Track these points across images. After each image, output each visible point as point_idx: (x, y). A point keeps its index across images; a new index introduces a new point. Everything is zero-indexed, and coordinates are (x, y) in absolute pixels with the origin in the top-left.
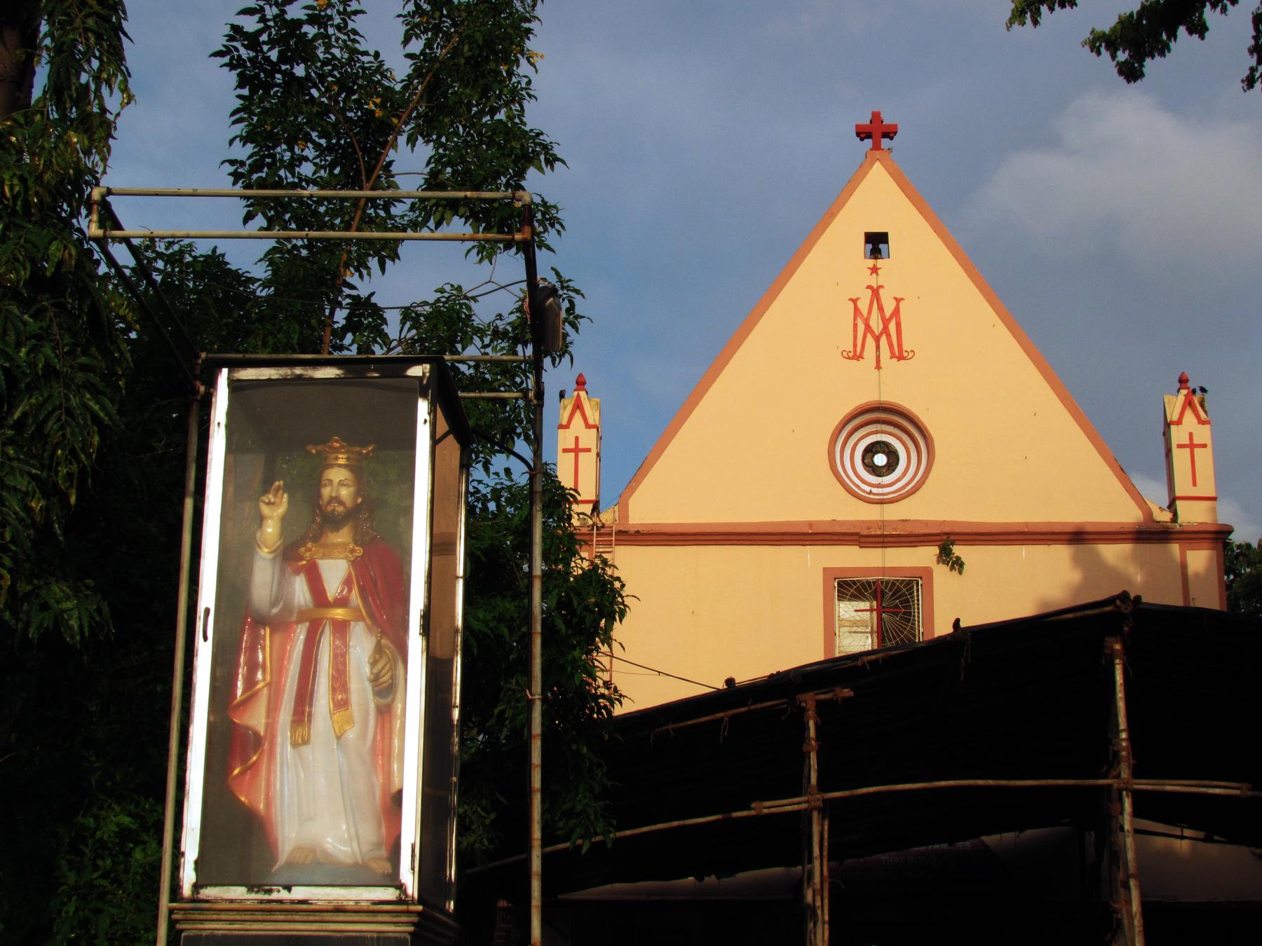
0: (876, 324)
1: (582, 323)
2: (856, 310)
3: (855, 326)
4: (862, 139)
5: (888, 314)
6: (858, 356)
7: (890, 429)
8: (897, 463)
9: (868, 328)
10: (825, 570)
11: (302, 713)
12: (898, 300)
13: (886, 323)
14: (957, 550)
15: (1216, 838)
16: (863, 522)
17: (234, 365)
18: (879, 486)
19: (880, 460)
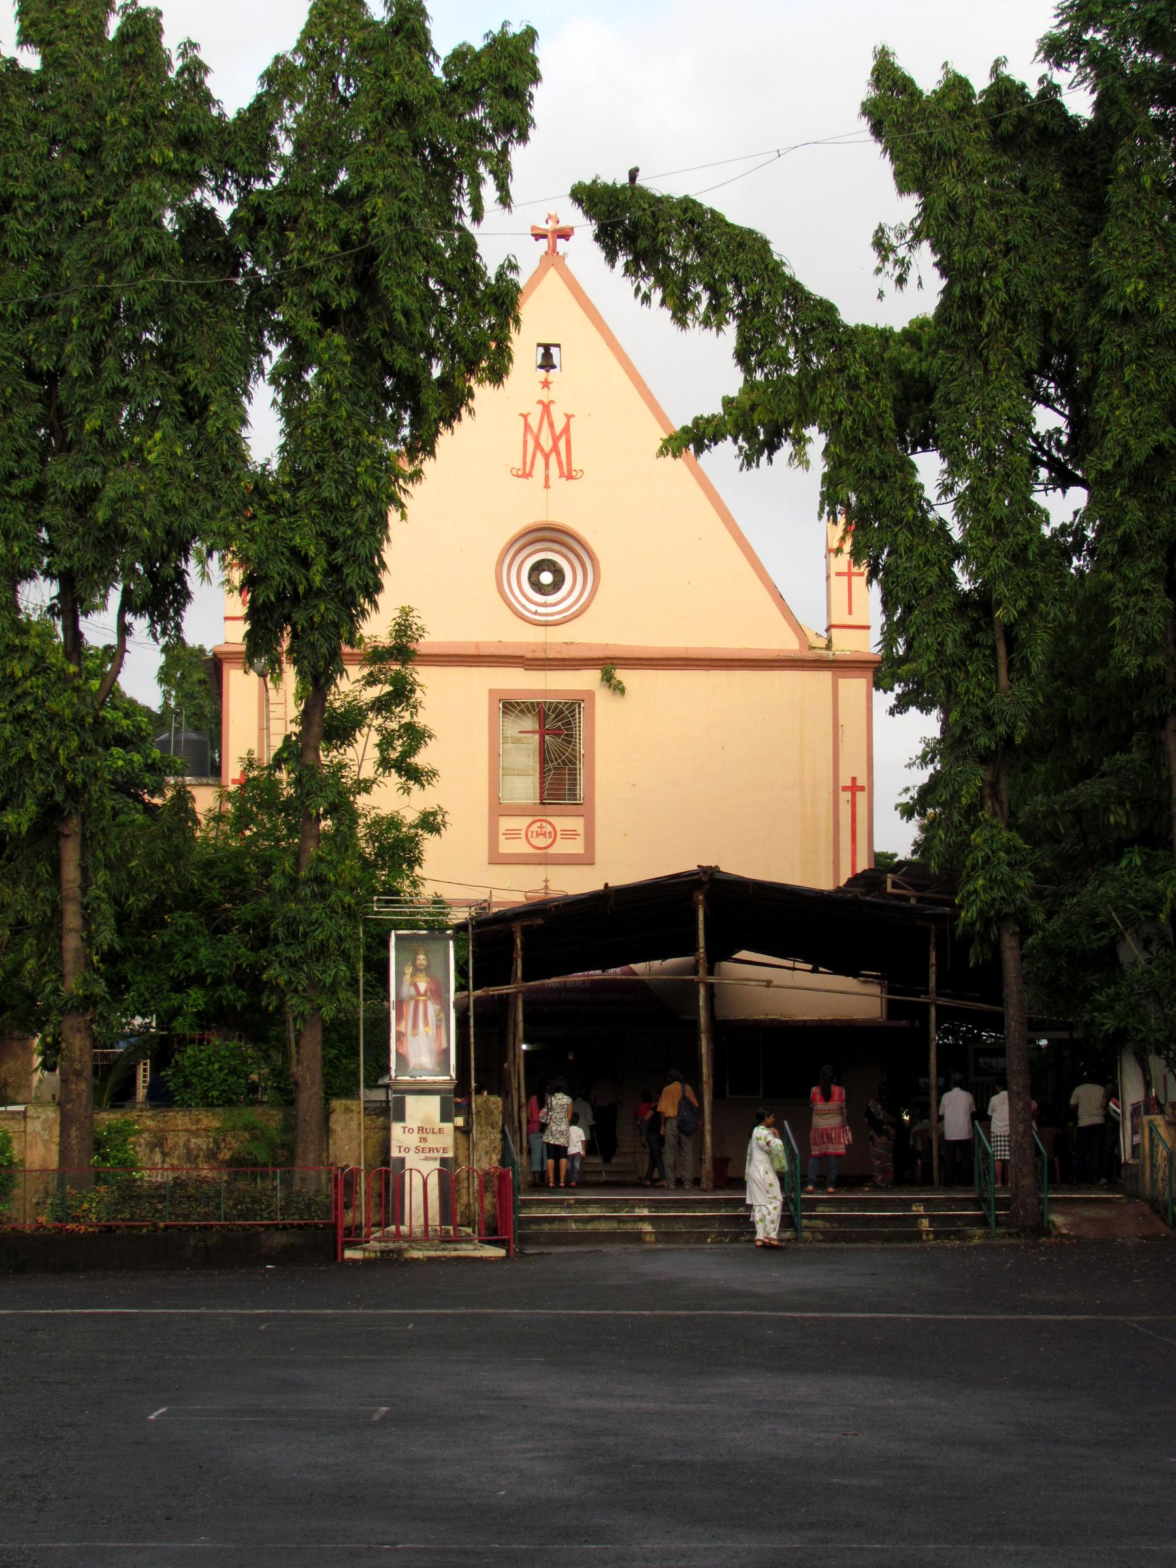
0: (546, 442)
1: (448, 826)
2: (527, 426)
3: (525, 443)
4: (537, 240)
5: (558, 430)
6: (527, 475)
7: (556, 547)
8: (563, 582)
9: (538, 445)
10: (491, 691)
11: (415, 1025)
12: (569, 417)
13: (556, 440)
14: (620, 674)
15: (821, 969)
16: (528, 644)
17: (396, 929)
18: (545, 605)
19: (546, 578)
